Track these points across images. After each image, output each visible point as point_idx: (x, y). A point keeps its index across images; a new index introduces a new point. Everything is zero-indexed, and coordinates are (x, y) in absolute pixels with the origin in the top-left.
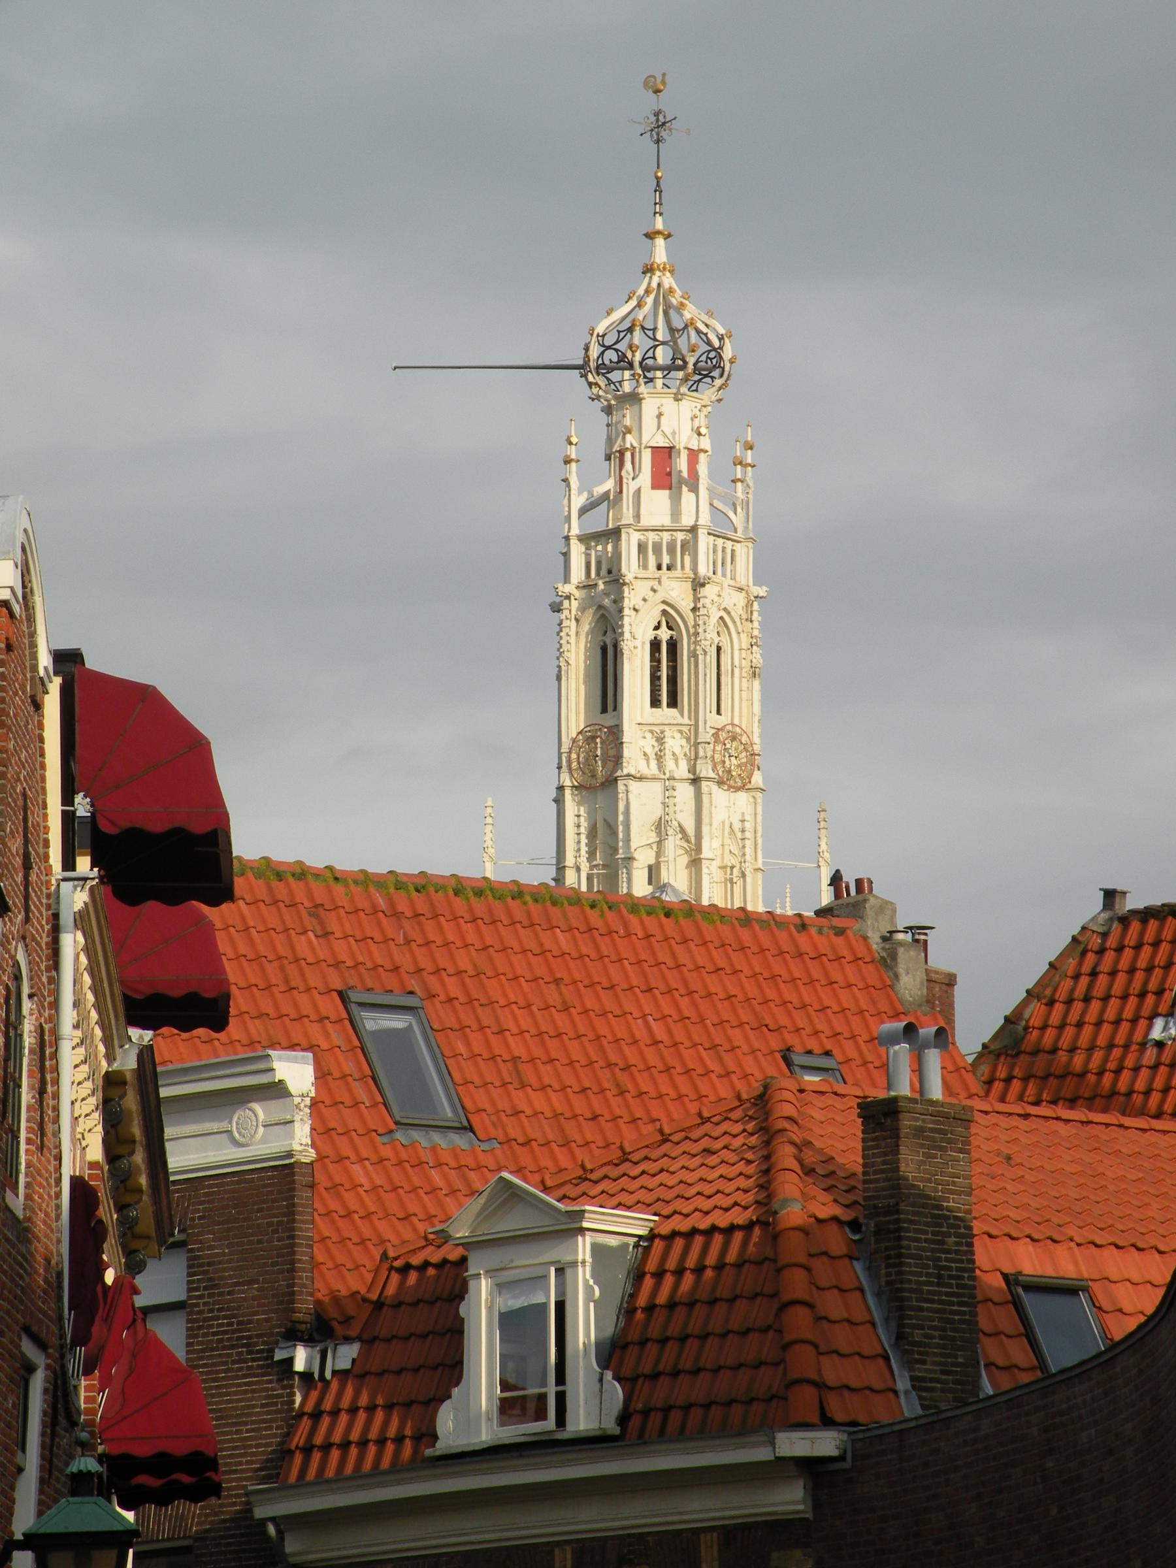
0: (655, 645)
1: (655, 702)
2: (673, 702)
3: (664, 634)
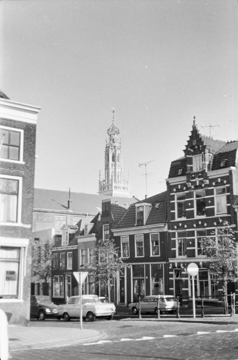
1: (113, 161)
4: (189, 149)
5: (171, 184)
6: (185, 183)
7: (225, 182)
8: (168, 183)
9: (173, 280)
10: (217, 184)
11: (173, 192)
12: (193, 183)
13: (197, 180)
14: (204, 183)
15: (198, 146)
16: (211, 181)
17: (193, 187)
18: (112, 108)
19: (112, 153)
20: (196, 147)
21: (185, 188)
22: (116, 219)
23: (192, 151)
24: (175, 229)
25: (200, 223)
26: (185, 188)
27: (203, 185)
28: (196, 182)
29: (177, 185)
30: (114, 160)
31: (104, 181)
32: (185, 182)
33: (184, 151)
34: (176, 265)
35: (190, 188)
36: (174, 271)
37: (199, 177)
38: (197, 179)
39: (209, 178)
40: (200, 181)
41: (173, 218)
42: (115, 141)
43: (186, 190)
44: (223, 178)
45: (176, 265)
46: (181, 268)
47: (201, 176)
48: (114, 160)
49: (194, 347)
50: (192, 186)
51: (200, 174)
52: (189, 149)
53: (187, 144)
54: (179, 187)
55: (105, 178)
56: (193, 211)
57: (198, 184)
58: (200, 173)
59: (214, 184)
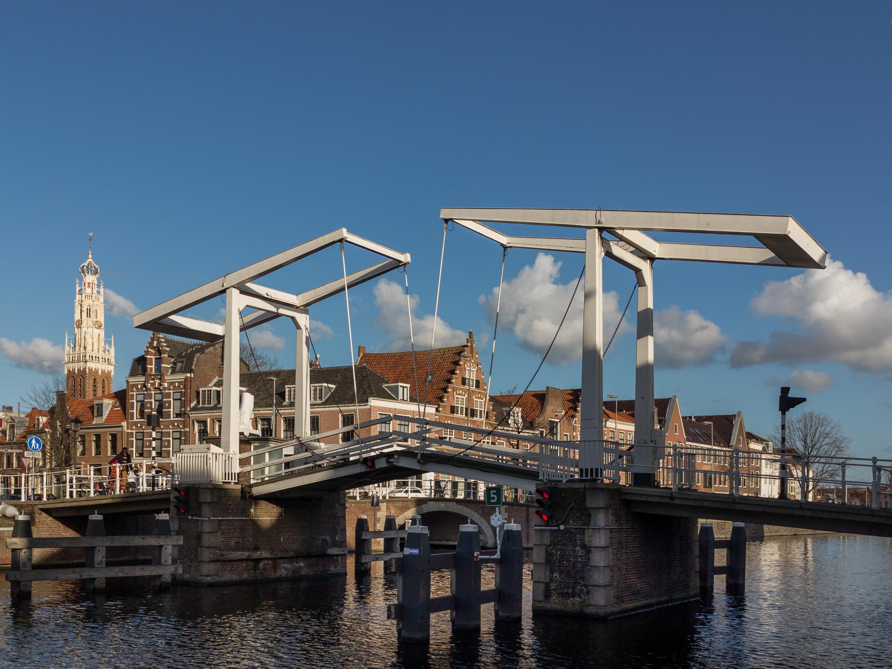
0: (87, 309)
2: (90, 317)
3: (89, 308)
7: (182, 387)
16: (170, 384)
24: (133, 430)
29: (138, 384)
30: (89, 315)
41: (132, 417)
48: (89, 315)
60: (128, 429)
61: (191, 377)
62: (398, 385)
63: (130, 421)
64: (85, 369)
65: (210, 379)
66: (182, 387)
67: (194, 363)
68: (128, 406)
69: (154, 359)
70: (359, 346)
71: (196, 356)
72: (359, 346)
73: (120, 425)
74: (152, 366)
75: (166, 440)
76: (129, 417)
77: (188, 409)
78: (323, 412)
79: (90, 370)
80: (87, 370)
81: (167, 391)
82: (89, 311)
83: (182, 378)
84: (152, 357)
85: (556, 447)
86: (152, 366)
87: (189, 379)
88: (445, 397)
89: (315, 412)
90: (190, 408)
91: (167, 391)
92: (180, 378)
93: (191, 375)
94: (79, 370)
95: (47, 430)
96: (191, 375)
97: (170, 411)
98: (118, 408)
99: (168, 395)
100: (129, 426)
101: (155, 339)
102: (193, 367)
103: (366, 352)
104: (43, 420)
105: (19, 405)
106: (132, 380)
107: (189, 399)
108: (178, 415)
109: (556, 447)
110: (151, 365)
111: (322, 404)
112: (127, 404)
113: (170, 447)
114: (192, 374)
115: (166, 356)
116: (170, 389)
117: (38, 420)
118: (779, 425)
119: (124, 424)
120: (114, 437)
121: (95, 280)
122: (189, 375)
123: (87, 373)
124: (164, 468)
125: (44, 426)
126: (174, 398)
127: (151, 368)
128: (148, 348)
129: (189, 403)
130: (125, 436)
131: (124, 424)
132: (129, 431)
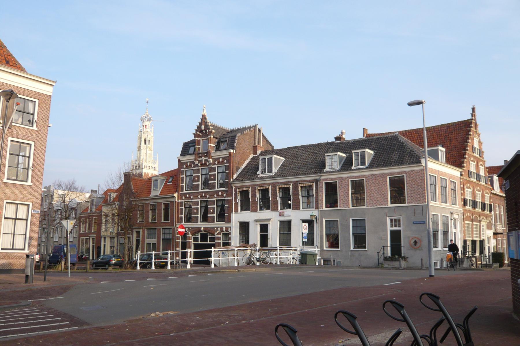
4: (198, 133)
5: (182, 162)
6: (193, 161)
7: (225, 161)
8: (179, 161)
9: (220, 242)
10: (219, 163)
11: (184, 168)
12: (200, 161)
13: (203, 159)
14: (208, 162)
15: (206, 131)
16: (215, 160)
17: (199, 165)
18: (147, 99)
19: (144, 138)
20: (204, 132)
21: (193, 165)
22: (135, 190)
23: (200, 134)
24: (183, 199)
25: (220, 193)
26: (193, 165)
27: (208, 164)
28: (202, 160)
29: (187, 162)
30: (145, 143)
31: (136, 161)
32: (193, 160)
33: (194, 134)
34: (224, 230)
35: (197, 166)
36: (222, 234)
37: (205, 156)
38: (203, 158)
39: (213, 158)
40: (205, 160)
41: (182, 190)
42: (147, 127)
43: (194, 167)
44: (224, 158)
45: (224, 230)
46: (228, 231)
47: (206, 156)
48: (145, 143)
49: (132, 262)
50: (198, 163)
51: (206, 154)
52: (198, 133)
53: (196, 128)
54: (189, 164)
55: (137, 158)
56: (428, 147)
57: (203, 163)
58: (206, 153)
59: (216, 163)
60: (178, 199)
61: (233, 153)
62: (438, 149)
63: (180, 192)
64: (142, 173)
65: (247, 155)
66: (225, 161)
67: (236, 141)
68: (179, 180)
69: (201, 140)
70: (364, 129)
71: (237, 135)
72: (364, 129)
73: (173, 196)
74: (199, 147)
75: (211, 207)
76: (180, 190)
77: (232, 180)
78: (368, 175)
79: (145, 174)
80: (143, 174)
81: (212, 166)
82: (145, 141)
83: (226, 154)
84: (200, 139)
85: (468, 214)
86: (199, 147)
87: (232, 154)
88: (465, 162)
89: (359, 176)
90: (233, 179)
91: (212, 166)
92: (224, 154)
93: (234, 151)
94: (138, 174)
95: (115, 203)
96: (234, 151)
97: (215, 183)
98: (170, 183)
99: (213, 170)
100: (180, 197)
101: (203, 123)
102: (235, 144)
103: (368, 133)
104: (114, 195)
105: (99, 186)
106: (184, 159)
107: (232, 172)
108: (222, 185)
109: (468, 214)
110: (199, 145)
111: (367, 168)
112: (179, 179)
113: (214, 214)
114: (235, 150)
115: (212, 136)
116: (214, 164)
117: (110, 195)
118: (423, 211)
119: (176, 195)
120: (167, 206)
121: (149, 124)
122: (232, 151)
123: (143, 175)
124: (209, 231)
125: (114, 201)
126: (218, 172)
127: (199, 148)
128: (196, 131)
129: (232, 175)
130: (176, 205)
131: (176, 195)
132: (180, 201)
